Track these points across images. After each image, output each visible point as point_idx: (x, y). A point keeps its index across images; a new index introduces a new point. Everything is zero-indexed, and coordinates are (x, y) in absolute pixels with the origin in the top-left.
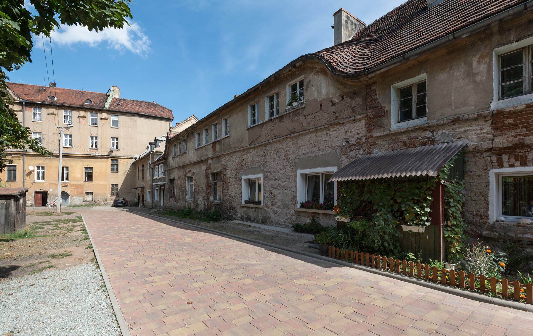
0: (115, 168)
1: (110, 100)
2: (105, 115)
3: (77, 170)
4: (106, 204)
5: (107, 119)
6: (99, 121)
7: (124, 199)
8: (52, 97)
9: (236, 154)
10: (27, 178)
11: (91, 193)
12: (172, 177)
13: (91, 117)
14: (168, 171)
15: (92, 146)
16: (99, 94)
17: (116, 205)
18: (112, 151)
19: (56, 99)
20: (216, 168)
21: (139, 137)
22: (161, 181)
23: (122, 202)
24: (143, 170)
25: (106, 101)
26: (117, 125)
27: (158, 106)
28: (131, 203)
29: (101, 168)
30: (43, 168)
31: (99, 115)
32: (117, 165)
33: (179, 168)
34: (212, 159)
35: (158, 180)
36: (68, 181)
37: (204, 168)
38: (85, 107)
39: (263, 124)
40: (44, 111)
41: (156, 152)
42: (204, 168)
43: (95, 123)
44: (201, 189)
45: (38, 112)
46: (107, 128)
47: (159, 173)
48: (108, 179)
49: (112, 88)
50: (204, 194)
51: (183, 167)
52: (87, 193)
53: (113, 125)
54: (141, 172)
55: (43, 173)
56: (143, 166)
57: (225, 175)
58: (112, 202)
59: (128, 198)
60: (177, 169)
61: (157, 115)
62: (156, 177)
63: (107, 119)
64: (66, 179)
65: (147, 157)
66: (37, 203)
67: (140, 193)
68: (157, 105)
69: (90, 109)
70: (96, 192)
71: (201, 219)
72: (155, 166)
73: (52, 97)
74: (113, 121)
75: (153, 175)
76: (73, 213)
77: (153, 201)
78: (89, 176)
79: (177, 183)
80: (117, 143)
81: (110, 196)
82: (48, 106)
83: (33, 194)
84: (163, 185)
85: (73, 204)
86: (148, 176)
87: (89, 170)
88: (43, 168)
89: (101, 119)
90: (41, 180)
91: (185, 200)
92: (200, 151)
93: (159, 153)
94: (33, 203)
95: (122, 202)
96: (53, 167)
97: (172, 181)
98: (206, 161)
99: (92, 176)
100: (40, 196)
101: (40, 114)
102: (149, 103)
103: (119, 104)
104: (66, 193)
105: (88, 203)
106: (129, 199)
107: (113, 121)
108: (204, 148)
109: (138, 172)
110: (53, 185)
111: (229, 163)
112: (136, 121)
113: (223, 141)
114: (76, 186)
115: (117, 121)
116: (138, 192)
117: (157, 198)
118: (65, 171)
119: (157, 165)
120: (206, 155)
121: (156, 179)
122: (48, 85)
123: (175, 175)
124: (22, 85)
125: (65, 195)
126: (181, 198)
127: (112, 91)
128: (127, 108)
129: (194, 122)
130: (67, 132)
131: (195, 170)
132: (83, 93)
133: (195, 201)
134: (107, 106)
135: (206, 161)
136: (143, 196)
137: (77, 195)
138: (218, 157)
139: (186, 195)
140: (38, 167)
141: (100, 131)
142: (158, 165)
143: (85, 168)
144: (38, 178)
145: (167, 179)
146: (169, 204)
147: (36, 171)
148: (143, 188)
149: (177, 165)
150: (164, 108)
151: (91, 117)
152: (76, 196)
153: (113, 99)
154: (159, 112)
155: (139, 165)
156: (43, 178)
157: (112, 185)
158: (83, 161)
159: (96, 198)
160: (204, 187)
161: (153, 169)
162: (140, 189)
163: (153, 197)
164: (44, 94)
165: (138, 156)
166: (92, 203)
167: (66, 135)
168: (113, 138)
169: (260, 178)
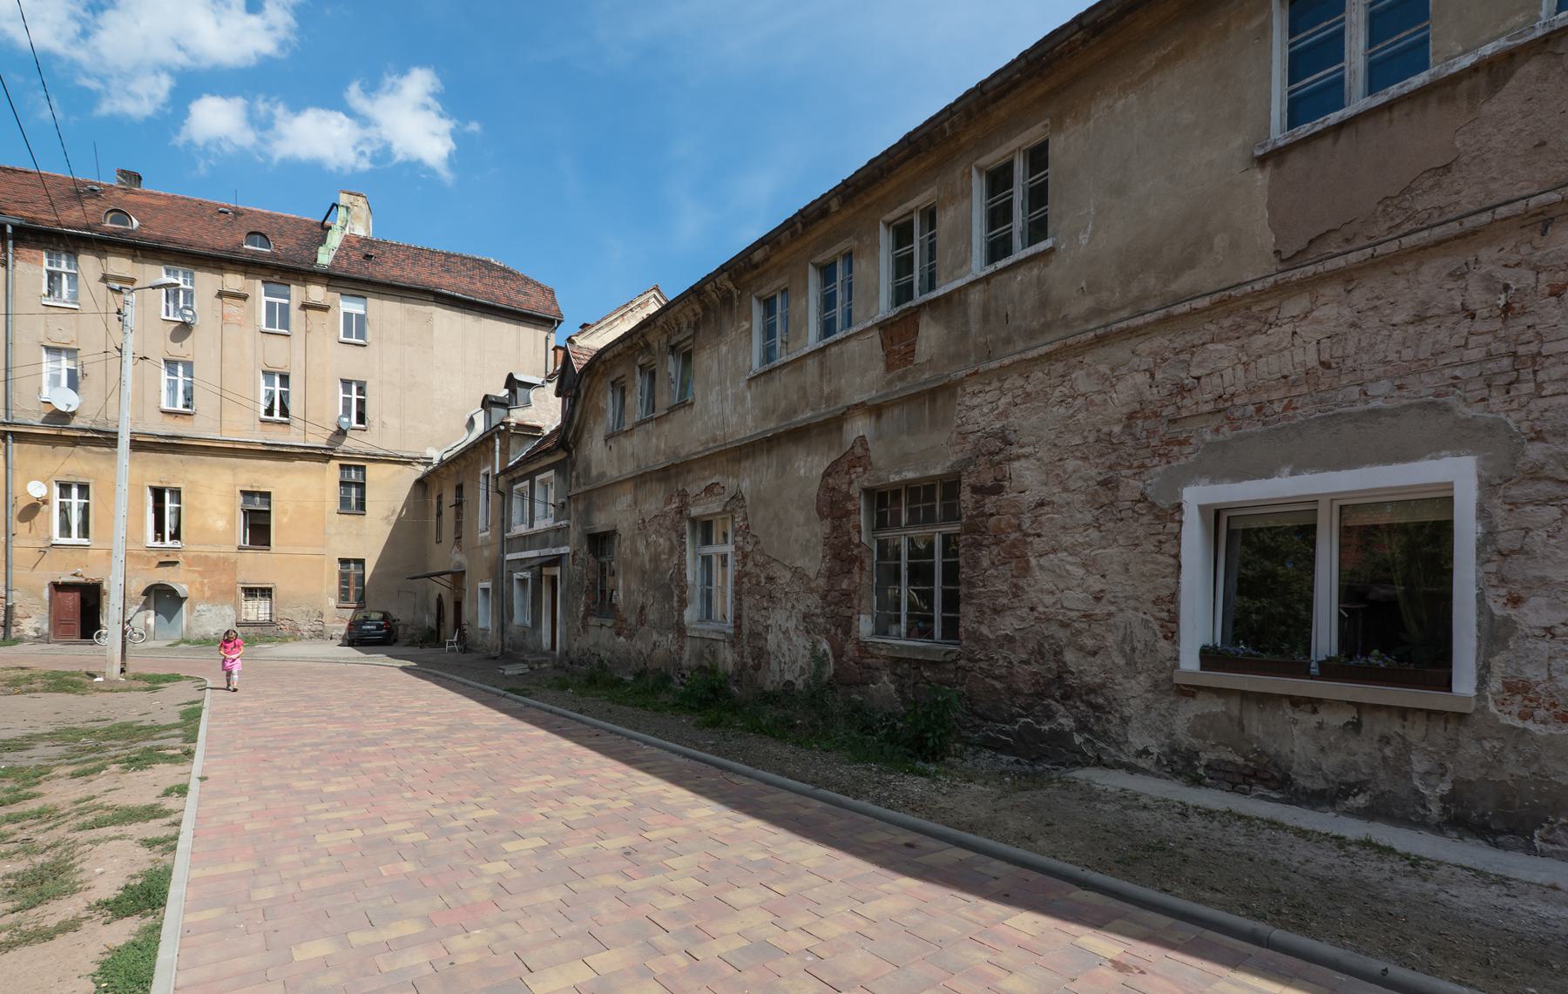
0: (354, 497)
1: (335, 239)
2: (317, 293)
3: (212, 501)
4: (319, 635)
5: (325, 309)
6: (295, 313)
7: (386, 616)
8: (121, 214)
9: (1120, 352)
10: (21, 528)
11: (266, 592)
12: (601, 522)
13: (264, 299)
14: (582, 496)
15: (270, 412)
16: (297, 222)
17: (357, 638)
18: (341, 433)
19: (136, 223)
20: (913, 454)
21: (441, 380)
22: (545, 545)
23: (379, 627)
24: (459, 505)
25: (323, 241)
26: (361, 334)
27: (507, 274)
28: (410, 631)
29: (303, 494)
30: (84, 489)
31: (297, 293)
32: (361, 486)
33: (642, 479)
34: (875, 410)
35: (526, 541)
36: (178, 544)
37: (809, 465)
38: (244, 257)
39: (1496, 70)
40: (89, 264)
41: (519, 426)
42: (809, 465)
43: (279, 317)
44: (784, 577)
45: (64, 267)
46: (325, 349)
47: (536, 512)
48: (329, 537)
49: (344, 199)
50: (813, 602)
51: (670, 473)
52: (251, 592)
53: (348, 333)
54: (449, 514)
55: (85, 510)
56: (459, 488)
57: (997, 489)
58: (341, 629)
59: (401, 614)
60: (629, 486)
61: (503, 304)
62: (520, 529)
63: (325, 309)
64: (172, 537)
65: (481, 447)
66: (57, 629)
67: (445, 592)
68: (504, 270)
69: (263, 266)
70: (281, 587)
71: (782, 730)
72: (514, 481)
73: (121, 214)
74: (348, 316)
75: (505, 523)
76: (177, 678)
77: (502, 629)
78: (258, 528)
79: (634, 548)
80: (361, 403)
81: (333, 602)
82: (103, 245)
83: (46, 593)
84: (556, 561)
85: (198, 632)
86: (481, 524)
87: (258, 505)
88: (84, 489)
89: (305, 307)
90: (75, 538)
91: (680, 629)
92: (783, 381)
93: (529, 431)
94: (46, 627)
95: (379, 627)
96: (124, 482)
97: (600, 542)
98: (832, 425)
99: (269, 526)
100: (72, 599)
101: (73, 278)
102: (475, 260)
103: (368, 257)
104: (173, 592)
105: (252, 631)
106: (407, 620)
107: (348, 316)
108: (812, 366)
109: (439, 514)
110: (118, 556)
111: (1024, 420)
112: (430, 320)
113: (975, 297)
114: (209, 565)
115: (361, 319)
116: (439, 588)
117: (521, 617)
118: (169, 505)
119: (522, 479)
120: (837, 395)
121: (522, 537)
122: (111, 179)
123: (617, 514)
124: (14, 171)
125: (163, 599)
126: (652, 615)
127: (342, 211)
128: (396, 272)
129: (653, 308)
130: (177, 350)
131: (749, 480)
132: (237, 213)
133: (746, 635)
134: (325, 258)
135: (832, 425)
136: (458, 606)
137: (212, 600)
138: (932, 394)
139: (683, 603)
140: (65, 488)
141: (299, 355)
142: (530, 476)
143: (244, 493)
144: (66, 529)
145: (574, 534)
146: (586, 642)
147: (56, 501)
148: (458, 576)
149: (629, 469)
150: (527, 281)
151: (264, 299)
152: (208, 600)
153: (347, 239)
154: (513, 295)
155: (443, 484)
156: (85, 530)
157: (344, 562)
158: (234, 468)
159: (285, 612)
160: (814, 564)
161: (505, 495)
162: (448, 577)
163: (504, 613)
164: (91, 206)
165: (436, 455)
166: (269, 631)
167: (171, 364)
168: (346, 384)
169: (911, 541)
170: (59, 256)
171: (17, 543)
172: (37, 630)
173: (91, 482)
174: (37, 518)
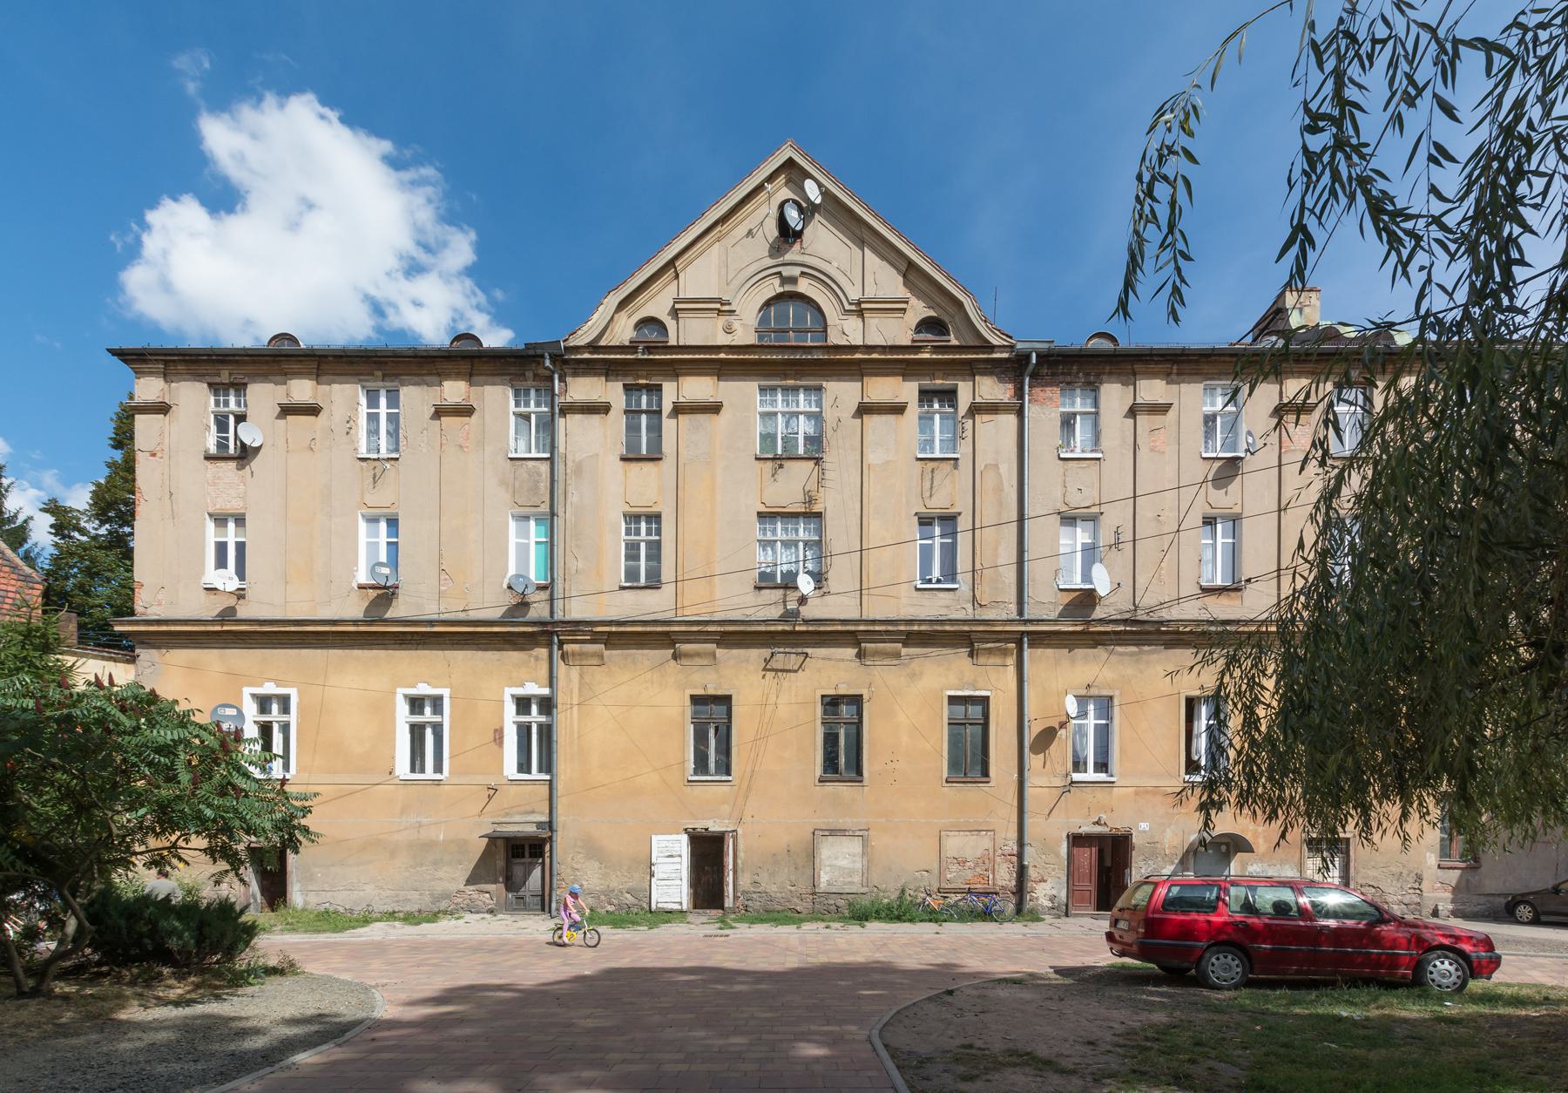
40: (1114, 396)
83: (1063, 849)
90: (535, 774)
100: (1087, 856)
130: (1224, 500)
170: (1073, 397)
171: (1032, 780)
172: (1052, 898)
173: (1116, 693)
174: (1053, 747)
